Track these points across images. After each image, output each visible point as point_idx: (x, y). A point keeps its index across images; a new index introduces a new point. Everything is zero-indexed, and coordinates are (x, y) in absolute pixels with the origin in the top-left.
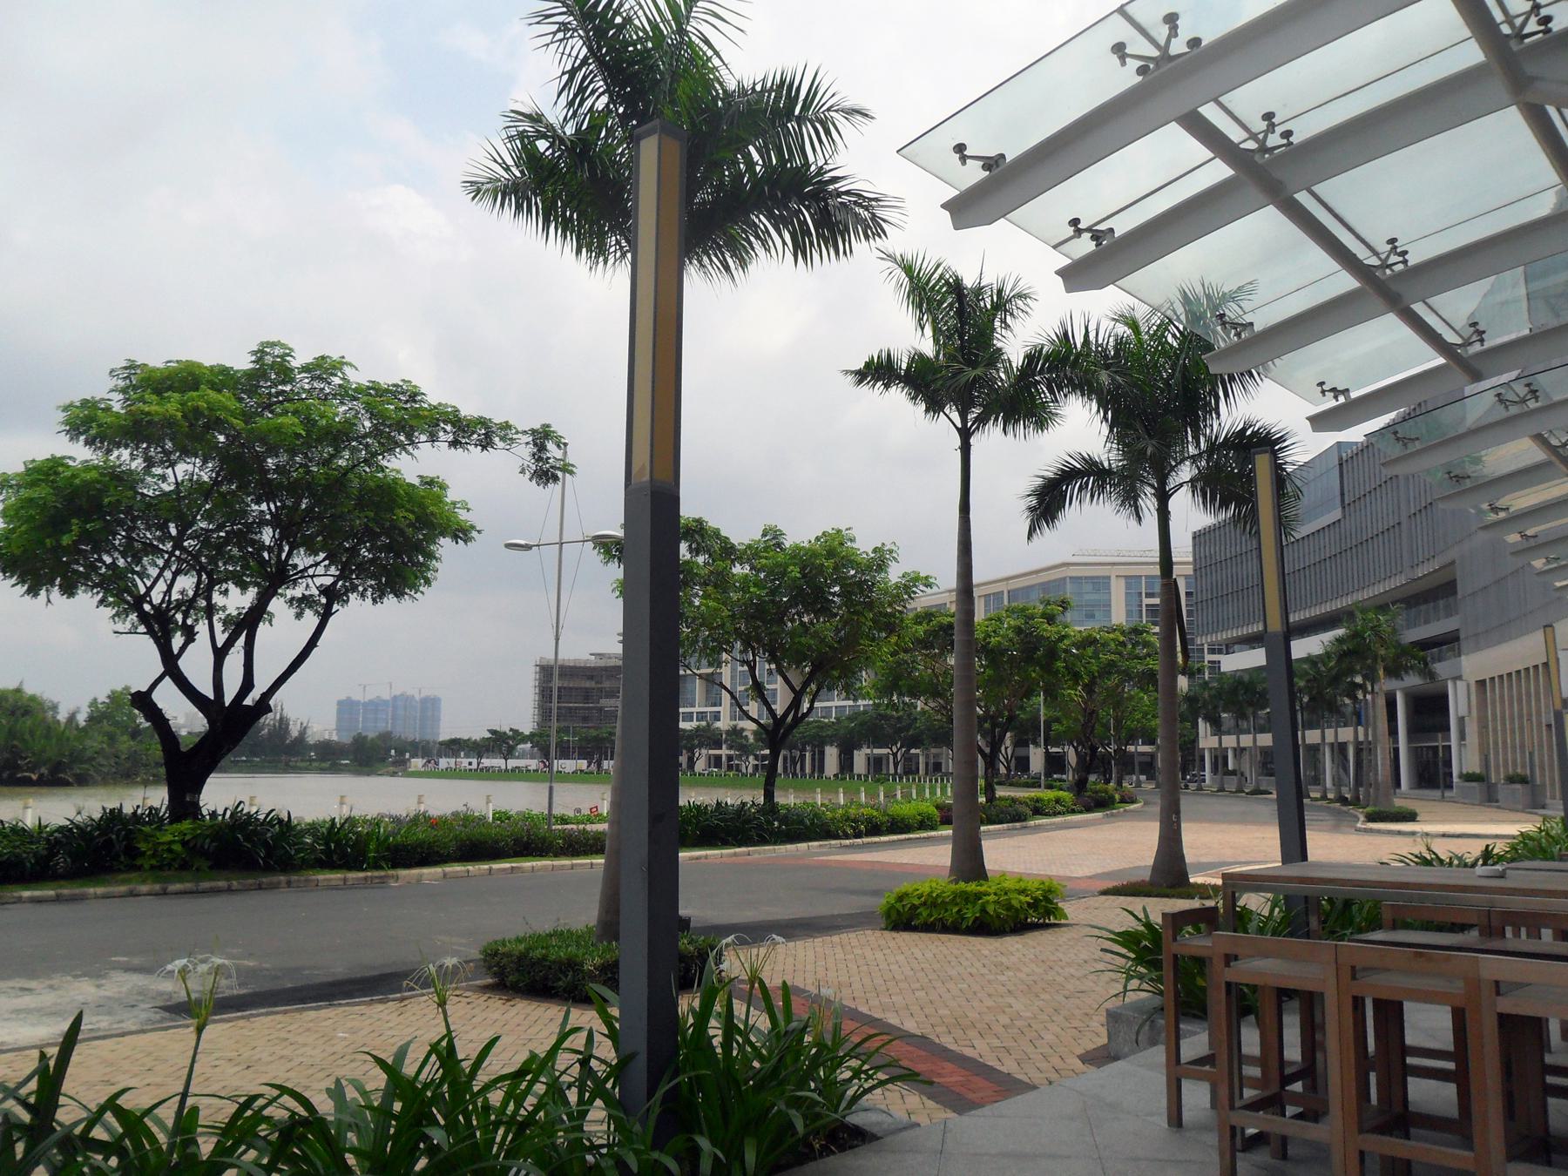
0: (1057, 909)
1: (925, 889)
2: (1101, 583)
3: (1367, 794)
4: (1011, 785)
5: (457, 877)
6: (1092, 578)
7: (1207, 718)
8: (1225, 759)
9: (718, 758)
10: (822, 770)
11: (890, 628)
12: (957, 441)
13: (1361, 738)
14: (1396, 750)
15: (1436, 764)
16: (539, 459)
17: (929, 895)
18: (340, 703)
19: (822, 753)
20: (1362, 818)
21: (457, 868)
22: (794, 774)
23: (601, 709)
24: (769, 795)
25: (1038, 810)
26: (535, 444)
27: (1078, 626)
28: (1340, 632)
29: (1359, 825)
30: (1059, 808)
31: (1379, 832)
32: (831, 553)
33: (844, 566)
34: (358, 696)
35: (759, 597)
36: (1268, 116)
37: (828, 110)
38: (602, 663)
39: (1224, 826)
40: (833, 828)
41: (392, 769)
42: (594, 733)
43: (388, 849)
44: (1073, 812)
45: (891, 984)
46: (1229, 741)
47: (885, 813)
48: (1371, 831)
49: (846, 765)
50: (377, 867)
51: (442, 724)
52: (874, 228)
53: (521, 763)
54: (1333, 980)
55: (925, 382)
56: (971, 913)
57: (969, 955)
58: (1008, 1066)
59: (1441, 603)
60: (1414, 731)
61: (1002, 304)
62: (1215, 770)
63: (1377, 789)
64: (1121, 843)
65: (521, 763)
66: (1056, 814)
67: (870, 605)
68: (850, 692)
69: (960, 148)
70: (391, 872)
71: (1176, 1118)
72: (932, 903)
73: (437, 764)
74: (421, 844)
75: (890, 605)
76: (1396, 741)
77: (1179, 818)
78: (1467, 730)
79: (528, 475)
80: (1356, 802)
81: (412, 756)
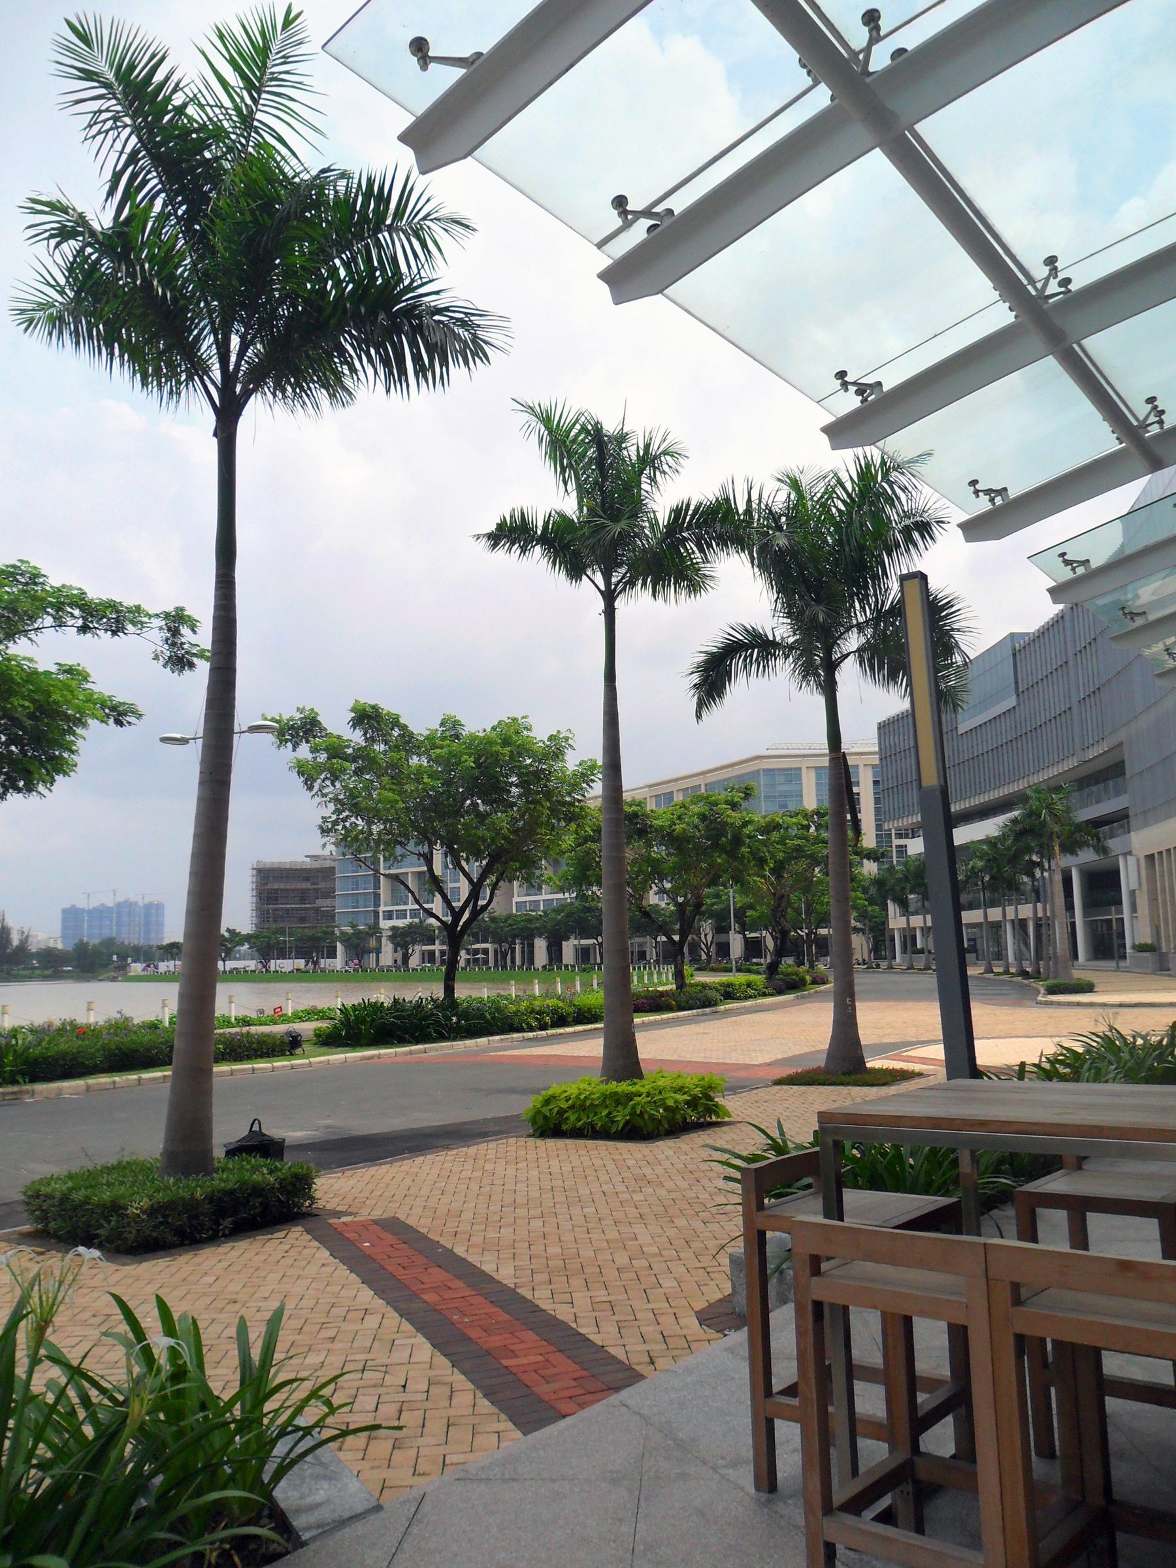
0: (716, 1105)
1: (573, 1090)
2: (793, 775)
3: (1048, 968)
4: (712, 970)
5: (102, 1089)
6: (783, 770)
7: (894, 900)
8: (914, 938)
9: (432, 953)
10: (531, 961)
11: (570, 818)
12: (600, 604)
13: (1040, 914)
14: (1073, 924)
15: (1110, 935)
16: (174, 644)
17: (578, 1097)
18: (64, 911)
19: (531, 946)
20: (1043, 991)
21: (103, 1080)
22: (504, 967)
23: (317, 910)
24: (449, 990)
25: (729, 994)
26: (169, 629)
27: (761, 811)
28: (1016, 813)
29: (1040, 998)
30: (751, 992)
31: (1059, 1004)
32: (506, 742)
33: (520, 754)
34: (82, 903)
35: (433, 788)
36: (871, 18)
37: (425, 218)
38: (317, 865)
39: (909, 1004)
40: (516, 1020)
41: (112, 974)
42: (309, 933)
43: (26, 1062)
44: (764, 995)
45: (589, 1172)
46: (917, 921)
47: (571, 1004)
48: (1052, 1003)
49: (555, 954)
50: (14, 1082)
51: (166, 929)
52: (475, 350)
53: (239, 964)
54: (981, 1304)
55: (568, 547)
56: (621, 1116)
57: (611, 1167)
58: (605, 1336)
59: (1111, 783)
60: (1088, 906)
61: (649, 460)
62: (904, 950)
63: (1056, 963)
64: (797, 1028)
65: (239, 964)
66: (747, 998)
67: (548, 795)
68: (533, 885)
69: (419, 47)
70: (28, 1087)
71: (767, 1480)
72: (582, 1106)
73: (156, 967)
74: (63, 1055)
75: (569, 794)
76: (1073, 916)
77: (853, 1002)
78: (1138, 902)
79: (162, 661)
80: (1037, 975)
81: (134, 961)
